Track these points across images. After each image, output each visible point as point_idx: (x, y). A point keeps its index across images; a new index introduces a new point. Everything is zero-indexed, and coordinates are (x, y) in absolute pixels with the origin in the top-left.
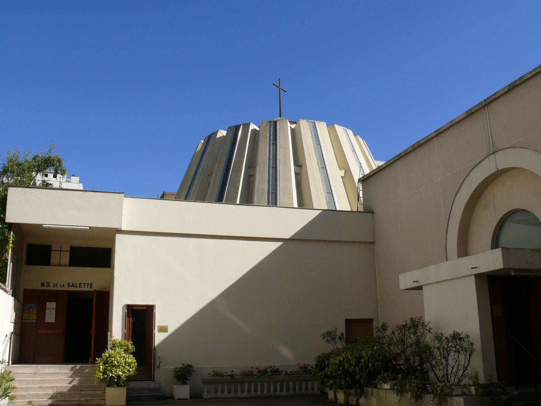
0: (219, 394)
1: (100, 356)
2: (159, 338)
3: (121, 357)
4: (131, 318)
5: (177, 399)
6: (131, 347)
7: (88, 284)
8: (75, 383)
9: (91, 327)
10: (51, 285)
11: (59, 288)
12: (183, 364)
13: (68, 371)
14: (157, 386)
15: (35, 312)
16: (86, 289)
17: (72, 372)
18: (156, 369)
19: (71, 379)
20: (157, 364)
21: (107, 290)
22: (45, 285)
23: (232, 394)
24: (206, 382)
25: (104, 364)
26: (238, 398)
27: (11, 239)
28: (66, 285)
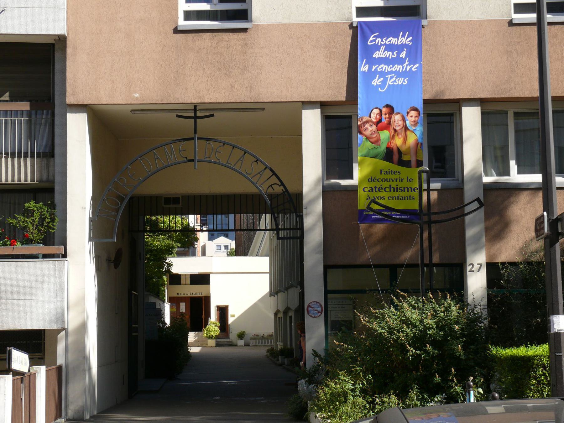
0: (257, 344)
1: (205, 328)
2: (231, 320)
3: (213, 328)
4: (219, 312)
5: (239, 346)
6: (218, 324)
7: (200, 293)
8: (196, 339)
9: (202, 314)
10: (182, 294)
11: (186, 296)
12: (241, 331)
13: (193, 334)
14: (231, 340)
15: (175, 308)
16: (199, 295)
17: (195, 335)
18: (230, 333)
19: (194, 337)
20: (230, 331)
21: (208, 296)
22: (179, 294)
23: (263, 344)
24: (251, 339)
25: (207, 331)
26: (265, 346)
27: (166, 280)
28: (189, 294)
